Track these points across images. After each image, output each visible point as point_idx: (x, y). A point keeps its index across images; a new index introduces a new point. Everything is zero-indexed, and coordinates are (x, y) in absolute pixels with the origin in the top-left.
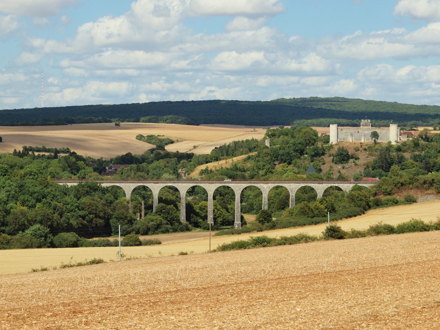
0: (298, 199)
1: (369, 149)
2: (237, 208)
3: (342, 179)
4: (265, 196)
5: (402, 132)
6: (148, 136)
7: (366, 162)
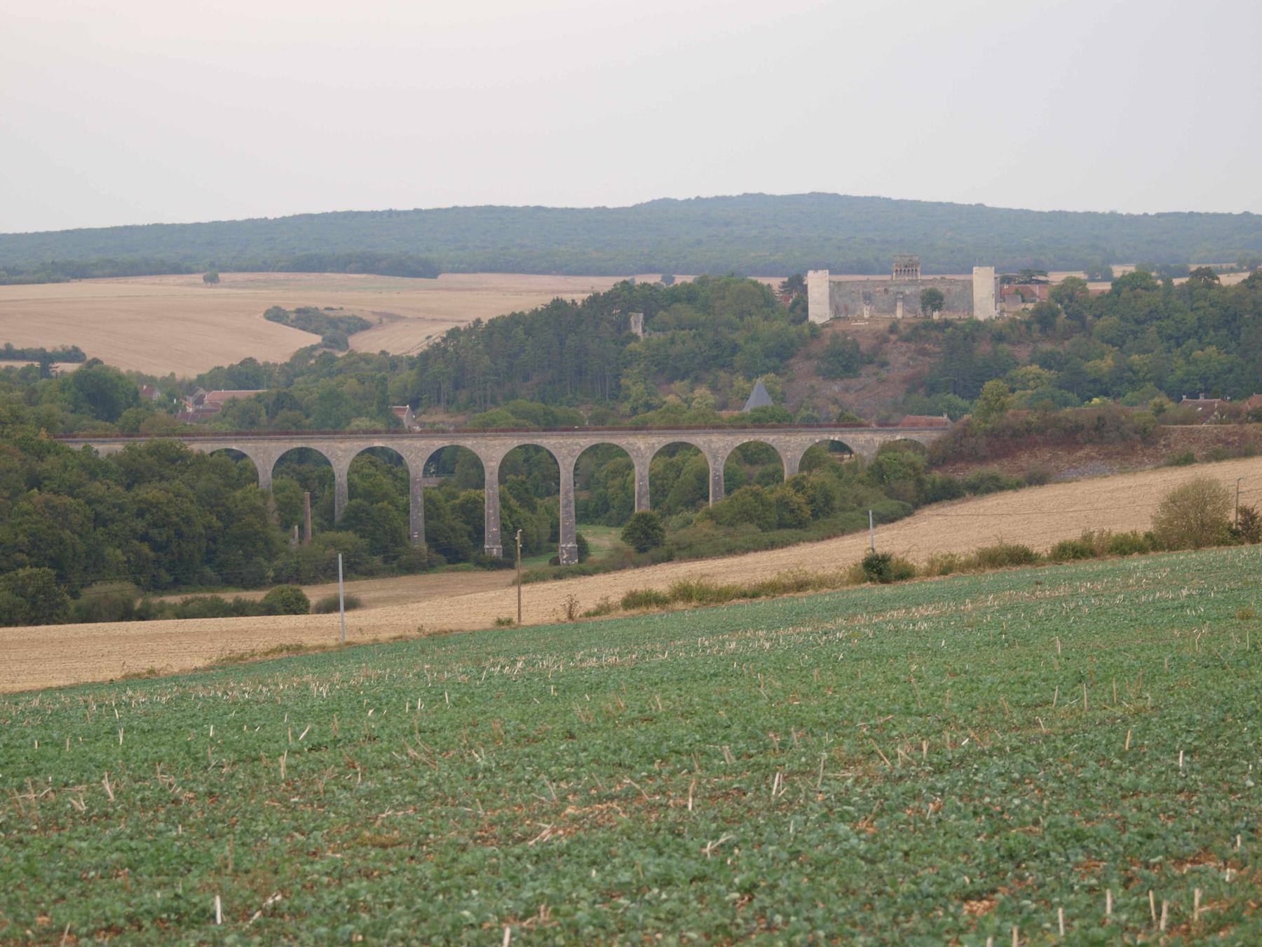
0: (731, 482)
1: (918, 333)
2: (566, 506)
3: (847, 422)
4: (641, 472)
5: (1006, 287)
6: (299, 311)
7: (909, 371)
